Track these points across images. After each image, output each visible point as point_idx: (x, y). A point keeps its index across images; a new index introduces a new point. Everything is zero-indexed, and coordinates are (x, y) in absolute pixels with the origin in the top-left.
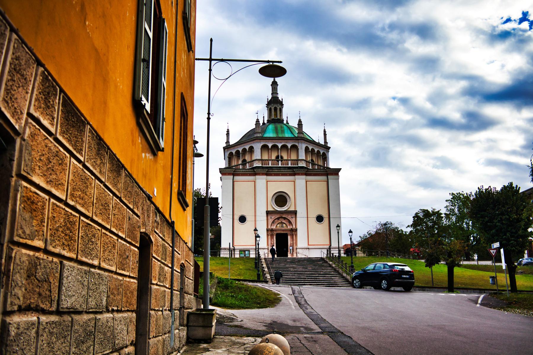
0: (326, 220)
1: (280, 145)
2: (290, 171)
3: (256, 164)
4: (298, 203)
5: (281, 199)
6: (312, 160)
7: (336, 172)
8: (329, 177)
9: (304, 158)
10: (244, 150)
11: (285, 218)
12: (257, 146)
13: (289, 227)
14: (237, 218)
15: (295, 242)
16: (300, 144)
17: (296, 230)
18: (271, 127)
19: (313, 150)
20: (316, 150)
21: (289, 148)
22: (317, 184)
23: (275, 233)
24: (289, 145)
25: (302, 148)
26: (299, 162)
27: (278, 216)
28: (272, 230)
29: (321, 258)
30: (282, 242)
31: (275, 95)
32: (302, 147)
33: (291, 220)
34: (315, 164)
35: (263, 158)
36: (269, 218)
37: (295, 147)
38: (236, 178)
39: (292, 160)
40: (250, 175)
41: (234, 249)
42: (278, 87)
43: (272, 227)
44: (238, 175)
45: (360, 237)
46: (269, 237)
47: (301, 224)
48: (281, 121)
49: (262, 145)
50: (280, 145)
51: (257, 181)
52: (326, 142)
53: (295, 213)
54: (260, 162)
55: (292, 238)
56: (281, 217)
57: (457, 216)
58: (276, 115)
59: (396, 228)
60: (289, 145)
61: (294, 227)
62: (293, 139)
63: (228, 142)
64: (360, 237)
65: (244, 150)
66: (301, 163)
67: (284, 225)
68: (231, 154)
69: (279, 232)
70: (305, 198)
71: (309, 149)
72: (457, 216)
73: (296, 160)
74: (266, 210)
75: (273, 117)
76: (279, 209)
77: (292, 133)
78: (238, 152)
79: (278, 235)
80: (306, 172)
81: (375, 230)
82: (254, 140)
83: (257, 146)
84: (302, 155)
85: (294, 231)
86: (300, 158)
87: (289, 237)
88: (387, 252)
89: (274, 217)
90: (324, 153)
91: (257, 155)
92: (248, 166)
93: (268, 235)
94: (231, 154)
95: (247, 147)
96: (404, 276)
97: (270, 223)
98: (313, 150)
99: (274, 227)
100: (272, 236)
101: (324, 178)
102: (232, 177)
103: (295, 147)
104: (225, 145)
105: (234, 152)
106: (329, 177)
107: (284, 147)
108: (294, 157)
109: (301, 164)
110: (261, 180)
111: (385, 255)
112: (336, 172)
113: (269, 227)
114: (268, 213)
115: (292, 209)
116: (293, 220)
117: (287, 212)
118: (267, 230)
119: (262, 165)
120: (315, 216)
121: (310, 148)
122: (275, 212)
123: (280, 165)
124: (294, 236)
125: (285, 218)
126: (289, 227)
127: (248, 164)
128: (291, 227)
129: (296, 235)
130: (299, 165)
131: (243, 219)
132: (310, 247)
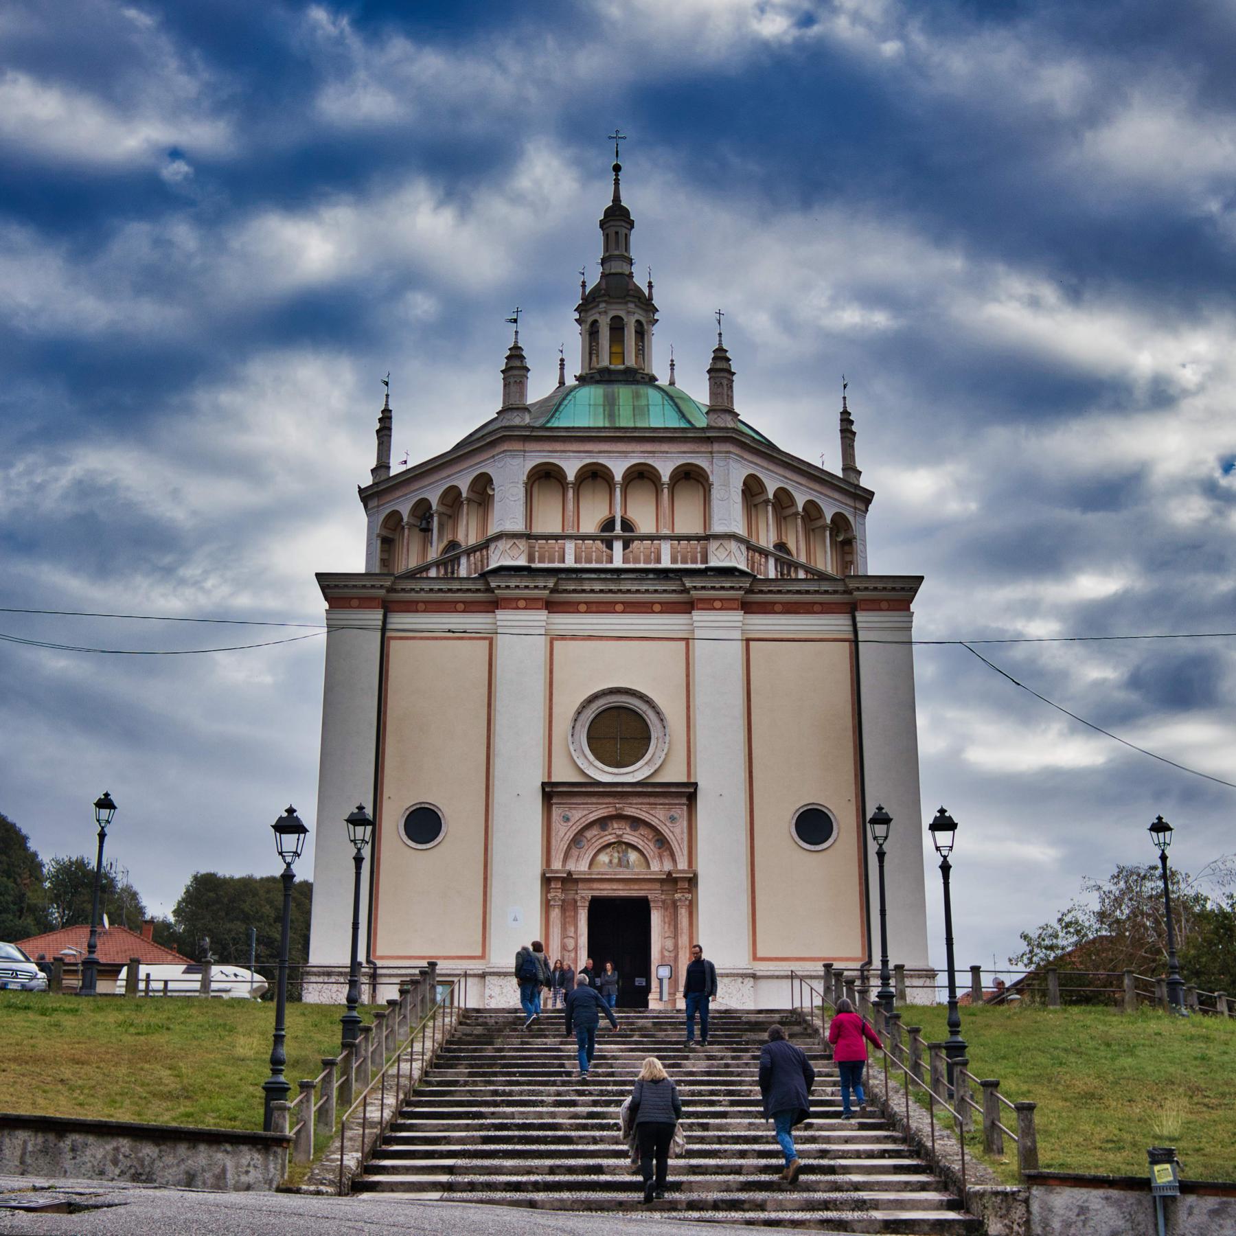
1: (618, 468)
2: (666, 591)
3: (500, 557)
4: (703, 743)
6: (781, 546)
7: (900, 593)
8: (861, 617)
9: (740, 529)
10: (452, 498)
11: (636, 823)
12: (510, 473)
13: (655, 866)
16: (719, 463)
17: (692, 881)
18: (592, 394)
19: (783, 497)
20: (800, 500)
21: (665, 478)
22: (802, 656)
23: (585, 894)
24: (665, 469)
25: (726, 484)
26: (713, 545)
27: (601, 812)
28: (569, 880)
29: (793, 1011)
31: (616, 267)
32: (727, 475)
33: (665, 830)
34: (797, 566)
35: (538, 529)
36: (556, 812)
37: (690, 477)
38: (400, 621)
39: (679, 538)
40: (470, 607)
42: (634, 236)
43: (571, 866)
44: (410, 607)
45: (1025, 937)
46: (555, 914)
47: (715, 846)
48: (639, 377)
49: (530, 464)
50: (618, 468)
51: (503, 643)
52: (850, 467)
53: (687, 794)
54: (522, 544)
55: (674, 923)
56: (620, 817)
59: (1197, 899)
60: (665, 469)
61: (682, 864)
62: (685, 440)
63: (382, 466)
64: (1025, 937)
65: (452, 498)
66: (722, 554)
67: (633, 856)
68: (393, 520)
69: (606, 891)
70: (741, 723)
73: (698, 538)
74: (538, 778)
75: (605, 362)
76: (604, 774)
77: (683, 416)
78: (422, 508)
80: (751, 596)
81: (1095, 904)
82: (492, 444)
83: (510, 473)
84: (729, 514)
85: (683, 885)
86: (717, 528)
87: (656, 918)
88: (1173, 985)
90: (840, 523)
91: (508, 511)
92: (463, 569)
93: (547, 906)
95: (464, 484)
97: (559, 846)
98: (783, 497)
99: (580, 866)
100: (568, 908)
101: (837, 624)
104: (368, 481)
105: (405, 509)
106: (861, 617)
107: (641, 476)
108: (687, 521)
109: (721, 557)
110: (522, 634)
111: (1155, 1002)
112: (900, 593)
113: (557, 865)
114: (551, 793)
116: (676, 833)
118: (547, 881)
119: (531, 559)
121: (771, 487)
122: (586, 790)
123: (618, 563)
124: (683, 912)
125: (636, 823)
126: (658, 867)
127: (463, 560)
128: (668, 866)
129: (692, 907)
130: (713, 563)
132: (762, 968)
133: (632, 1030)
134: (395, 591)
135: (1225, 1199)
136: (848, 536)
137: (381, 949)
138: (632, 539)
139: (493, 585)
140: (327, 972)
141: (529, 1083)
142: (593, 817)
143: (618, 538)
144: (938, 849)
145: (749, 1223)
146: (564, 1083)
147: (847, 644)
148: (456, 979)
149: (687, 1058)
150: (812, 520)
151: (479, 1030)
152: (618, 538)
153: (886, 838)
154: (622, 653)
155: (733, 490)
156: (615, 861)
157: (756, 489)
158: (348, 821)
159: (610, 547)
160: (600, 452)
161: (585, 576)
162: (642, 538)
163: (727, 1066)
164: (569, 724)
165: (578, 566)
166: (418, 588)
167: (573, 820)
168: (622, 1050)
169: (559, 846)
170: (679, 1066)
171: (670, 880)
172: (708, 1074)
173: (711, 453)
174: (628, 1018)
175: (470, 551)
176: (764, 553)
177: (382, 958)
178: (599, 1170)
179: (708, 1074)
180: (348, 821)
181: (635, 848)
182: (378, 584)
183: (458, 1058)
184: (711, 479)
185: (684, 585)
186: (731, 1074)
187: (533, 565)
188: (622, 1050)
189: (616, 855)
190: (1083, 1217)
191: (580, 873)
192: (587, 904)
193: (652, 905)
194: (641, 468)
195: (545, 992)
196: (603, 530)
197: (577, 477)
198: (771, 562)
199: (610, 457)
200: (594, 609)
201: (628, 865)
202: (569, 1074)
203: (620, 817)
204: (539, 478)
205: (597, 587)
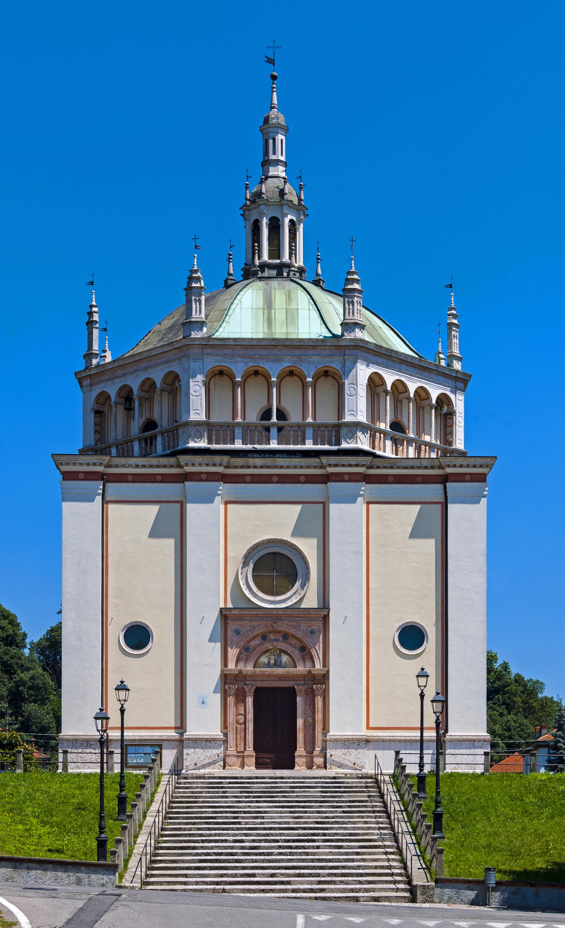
0: (431, 646)
10: (149, 386)
14: (116, 634)
15: (319, 716)
17: (324, 678)
43: (241, 666)
46: (231, 700)
58: (275, 252)
65: (149, 386)
68: (104, 397)
79: (259, 694)
94: (104, 397)
96: (148, 450)
100: (240, 698)
102: (447, 765)
105: (113, 390)
117: (296, 613)
120: (392, 633)
126: (301, 669)
134: (110, 466)
135: (518, 887)
140: (82, 743)
145: (316, 898)
147: (440, 506)
152: (274, 424)
153: (425, 686)
155: (359, 387)
156: (272, 662)
158: (116, 689)
178: (254, 875)
180: (116, 689)
181: (286, 653)
189: (273, 657)
190: (457, 895)
195: (196, 316)
196: (262, 419)
200: (256, 480)
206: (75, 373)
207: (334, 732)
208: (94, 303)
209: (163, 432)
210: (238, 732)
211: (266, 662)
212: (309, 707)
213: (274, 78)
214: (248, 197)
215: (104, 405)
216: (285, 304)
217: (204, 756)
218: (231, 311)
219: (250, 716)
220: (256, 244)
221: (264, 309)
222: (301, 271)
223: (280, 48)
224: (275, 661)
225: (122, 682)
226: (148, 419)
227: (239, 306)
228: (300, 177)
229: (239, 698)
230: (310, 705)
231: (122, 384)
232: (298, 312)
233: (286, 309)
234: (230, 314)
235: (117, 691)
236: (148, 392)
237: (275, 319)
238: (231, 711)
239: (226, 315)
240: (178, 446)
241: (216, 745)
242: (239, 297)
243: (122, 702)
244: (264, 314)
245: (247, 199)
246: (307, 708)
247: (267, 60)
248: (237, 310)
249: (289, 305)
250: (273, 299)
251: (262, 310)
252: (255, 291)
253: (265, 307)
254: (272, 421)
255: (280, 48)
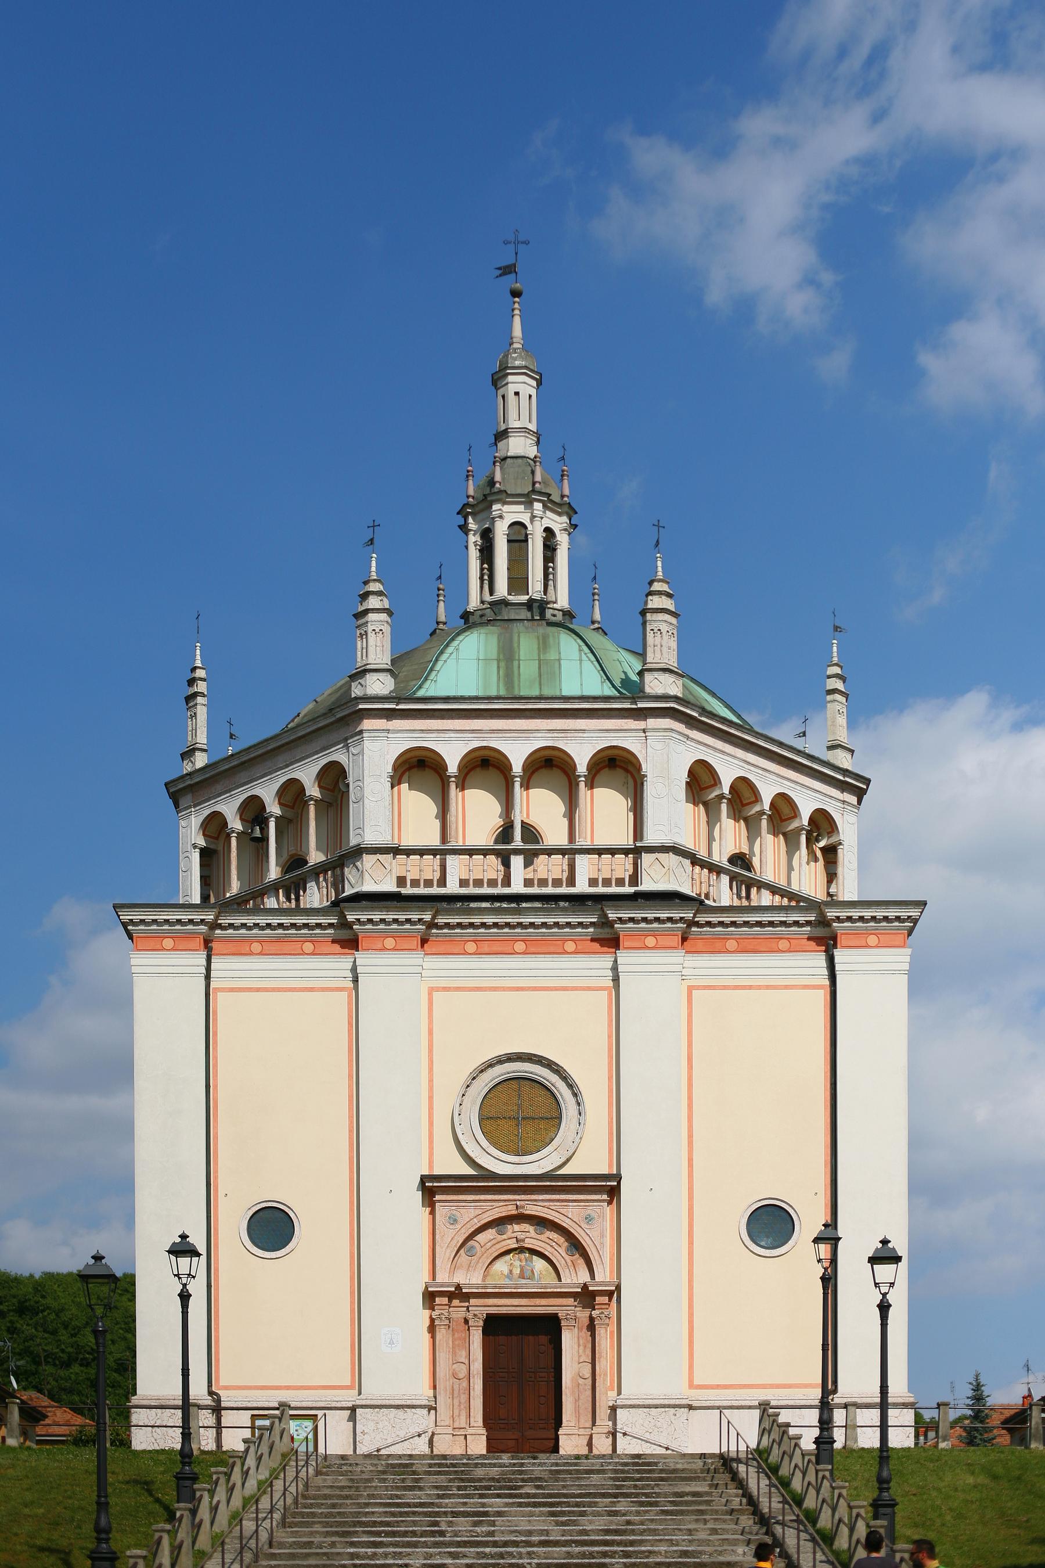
5: (523, 1100)
11: (542, 1223)
17: (614, 1293)
20: (767, 794)
28: (458, 1294)
30: (522, 1361)
41: (217, 1409)
56: (521, 1218)
57: (729, 799)
67: (539, 1264)
71: (795, 812)
72: (729, 799)
76: (500, 1163)
78: (254, 812)
79: (494, 1325)
84: (671, 816)
89: (472, 1211)
97: (444, 1254)
99: (471, 1278)
103: (618, 767)
109: (658, 875)
115: (591, 1161)
116: (596, 1237)
118: (430, 1297)
122: (483, 1183)
123: (517, 887)
125: (542, 1223)
126: (575, 1277)
128: (584, 1277)
130: (647, 885)
131: (272, 1228)
133: (523, 1480)
136: (833, 840)
137: (225, 1377)
138: (536, 853)
139: (350, 918)
141: (396, 1545)
142: (487, 1218)
143: (517, 852)
144: (876, 1285)
146: (436, 1545)
148: (320, 1413)
149: (583, 1514)
150: (782, 821)
151: (343, 1481)
152: (517, 852)
154: (534, 1001)
156: (517, 1271)
157: (705, 778)
158: (169, 1252)
159: (506, 864)
160: (493, 731)
161: (473, 905)
162: (550, 852)
163: (628, 1523)
164: (455, 1099)
165: (464, 891)
166: (250, 922)
167: (462, 1221)
168: (507, 1505)
169: (444, 1254)
170: (574, 1523)
171: (586, 1297)
172: (607, 1532)
173: (644, 731)
174: (522, 1465)
175: (320, 870)
176: (715, 869)
177: (226, 1388)
179: (607, 1532)
180: (169, 1252)
182: (197, 917)
183: (313, 1515)
184: (644, 766)
185: (606, 916)
186: (633, 1532)
187: (403, 891)
188: (507, 1505)
189: (517, 1263)
191: (471, 1286)
192: (481, 1323)
193: (563, 1323)
194: (547, 753)
196: (496, 842)
197: (460, 768)
198: (725, 879)
199: (506, 739)
200: (486, 949)
201: (532, 1277)
202: (442, 1533)
203: (521, 1218)
204: (410, 769)
205: (490, 920)
206: (166, 784)
207: (633, 1388)
208: (198, 663)
209: (318, 870)
210: (455, 1395)
211: (506, 1272)
212: (584, 1351)
213: (516, 294)
214: (471, 492)
215: (217, 838)
216: (536, 651)
217: (394, 1435)
218: (440, 663)
219: (478, 1366)
220: (486, 566)
221: (498, 661)
222: (568, 614)
223: (526, 243)
224: (522, 1270)
225: (184, 1237)
226: (292, 856)
227: (454, 656)
228: (563, 458)
229: (456, 1335)
230: (585, 1347)
231: (245, 796)
232: (560, 665)
233: (540, 660)
234: (437, 667)
235: (173, 1258)
236: (292, 807)
237: (519, 674)
238: (442, 1357)
239: (432, 670)
240: (343, 892)
241: (415, 1416)
242: (455, 643)
243: (184, 1281)
244: (498, 667)
245: (468, 497)
246: (581, 1351)
247: (500, 272)
248: (452, 662)
249: (545, 653)
250: (516, 645)
251: (495, 662)
252: (482, 636)
253: (501, 657)
254: (513, 841)
255: (526, 243)
